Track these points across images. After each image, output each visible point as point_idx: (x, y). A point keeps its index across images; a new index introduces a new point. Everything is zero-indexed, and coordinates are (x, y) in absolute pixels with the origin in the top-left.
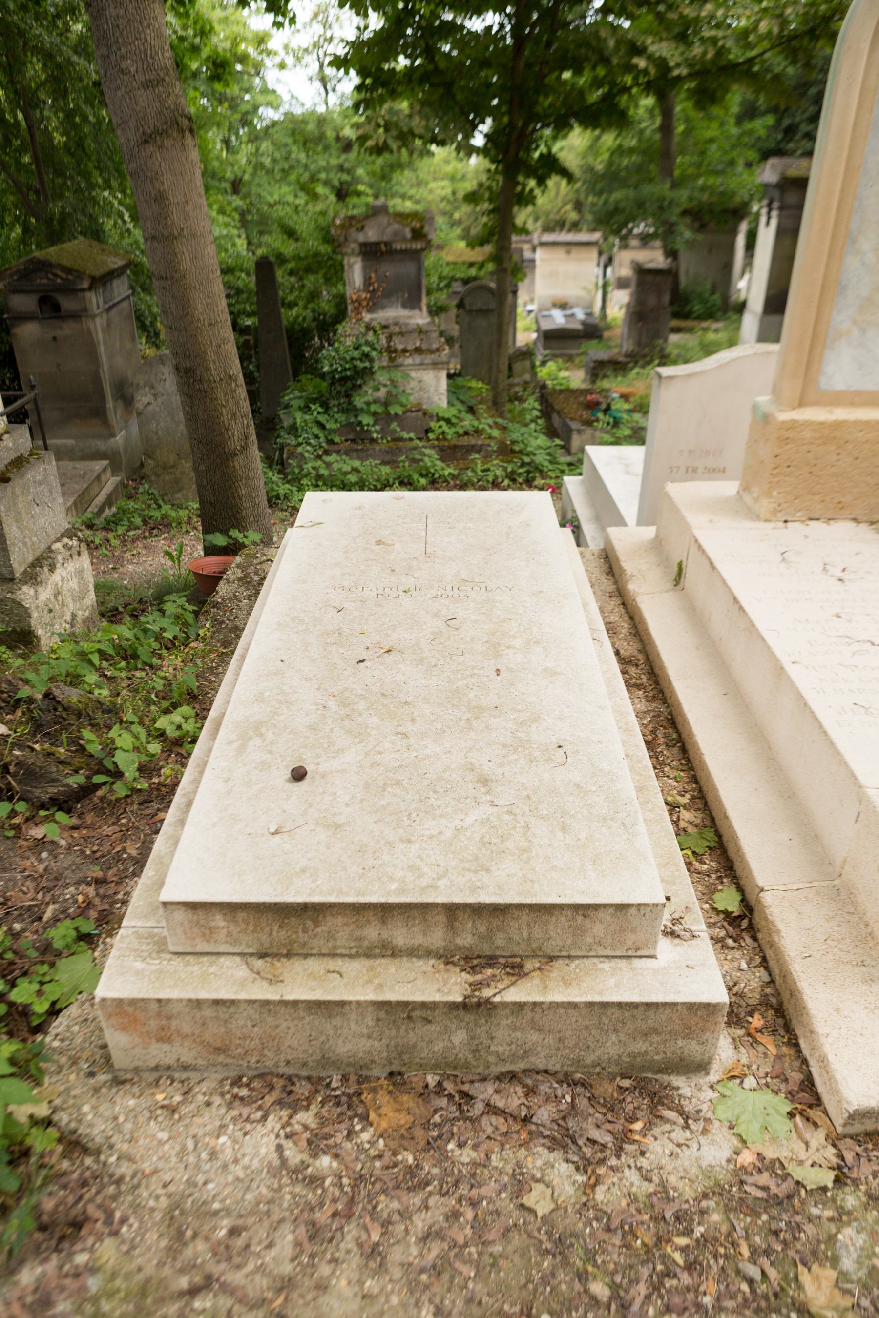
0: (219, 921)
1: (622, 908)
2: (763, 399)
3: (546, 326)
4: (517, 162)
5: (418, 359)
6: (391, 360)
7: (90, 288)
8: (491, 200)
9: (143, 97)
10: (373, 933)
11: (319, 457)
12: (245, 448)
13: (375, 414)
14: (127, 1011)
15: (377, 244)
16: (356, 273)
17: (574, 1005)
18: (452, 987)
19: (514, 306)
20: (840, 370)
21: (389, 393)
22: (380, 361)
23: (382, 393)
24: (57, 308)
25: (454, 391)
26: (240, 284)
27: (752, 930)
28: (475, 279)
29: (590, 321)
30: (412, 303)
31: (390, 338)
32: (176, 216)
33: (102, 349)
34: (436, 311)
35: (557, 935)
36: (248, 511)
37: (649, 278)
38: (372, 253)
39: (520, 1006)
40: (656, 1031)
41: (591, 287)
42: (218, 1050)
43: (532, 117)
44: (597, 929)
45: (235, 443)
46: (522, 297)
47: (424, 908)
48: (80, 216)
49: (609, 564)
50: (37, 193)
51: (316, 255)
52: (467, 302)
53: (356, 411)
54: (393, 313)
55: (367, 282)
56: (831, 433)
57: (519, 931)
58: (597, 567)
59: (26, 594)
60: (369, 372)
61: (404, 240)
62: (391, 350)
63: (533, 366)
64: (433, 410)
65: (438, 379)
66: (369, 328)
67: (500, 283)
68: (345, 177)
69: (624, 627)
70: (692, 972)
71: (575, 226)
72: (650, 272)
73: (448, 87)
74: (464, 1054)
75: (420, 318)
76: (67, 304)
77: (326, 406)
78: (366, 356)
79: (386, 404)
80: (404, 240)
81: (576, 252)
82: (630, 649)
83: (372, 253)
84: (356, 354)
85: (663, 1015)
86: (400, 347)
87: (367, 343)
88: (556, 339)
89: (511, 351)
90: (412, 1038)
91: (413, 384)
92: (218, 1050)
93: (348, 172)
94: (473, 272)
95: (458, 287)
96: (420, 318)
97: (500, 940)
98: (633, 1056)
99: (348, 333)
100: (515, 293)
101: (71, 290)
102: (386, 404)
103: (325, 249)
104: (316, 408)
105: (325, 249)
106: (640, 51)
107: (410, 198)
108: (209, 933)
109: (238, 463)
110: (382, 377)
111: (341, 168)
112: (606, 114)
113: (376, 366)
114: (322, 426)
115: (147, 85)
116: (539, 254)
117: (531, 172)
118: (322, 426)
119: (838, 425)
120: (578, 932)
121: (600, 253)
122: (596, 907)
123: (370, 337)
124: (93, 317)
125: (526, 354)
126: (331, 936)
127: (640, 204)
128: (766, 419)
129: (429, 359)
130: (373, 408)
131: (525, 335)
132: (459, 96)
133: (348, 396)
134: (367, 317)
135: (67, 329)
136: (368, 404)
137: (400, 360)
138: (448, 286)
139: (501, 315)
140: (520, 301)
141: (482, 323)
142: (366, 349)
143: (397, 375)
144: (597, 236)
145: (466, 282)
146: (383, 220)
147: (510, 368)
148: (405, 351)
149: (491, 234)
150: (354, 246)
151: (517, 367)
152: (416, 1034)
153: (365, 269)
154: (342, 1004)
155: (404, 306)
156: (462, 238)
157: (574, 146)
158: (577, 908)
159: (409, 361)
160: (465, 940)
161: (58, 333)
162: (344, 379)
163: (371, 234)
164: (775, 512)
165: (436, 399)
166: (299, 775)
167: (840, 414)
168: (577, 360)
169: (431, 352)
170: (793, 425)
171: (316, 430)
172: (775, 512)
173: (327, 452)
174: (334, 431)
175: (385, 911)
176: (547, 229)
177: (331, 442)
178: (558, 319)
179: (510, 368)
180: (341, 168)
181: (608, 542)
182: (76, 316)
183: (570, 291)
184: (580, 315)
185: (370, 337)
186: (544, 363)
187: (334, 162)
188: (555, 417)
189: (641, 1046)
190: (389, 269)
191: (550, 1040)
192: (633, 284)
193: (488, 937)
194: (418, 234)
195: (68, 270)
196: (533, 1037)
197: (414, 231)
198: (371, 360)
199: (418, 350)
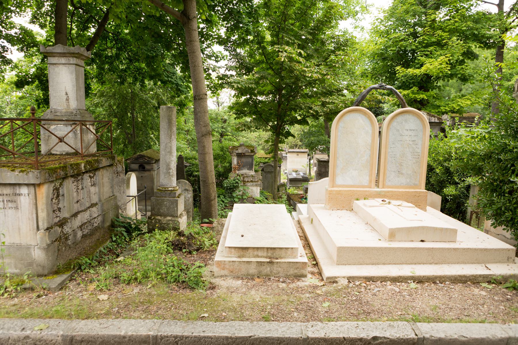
0: (233, 250)
1: (292, 248)
2: (327, 187)
3: (290, 177)
4: (279, 134)
5: (251, 184)
6: (244, 184)
7: (155, 163)
8: (272, 142)
9: (203, 129)
10: (256, 253)
11: (222, 210)
12: (215, 199)
13: (239, 198)
14: (219, 263)
15: (241, 153)
16: (235, 161)
17: (285, 262)
18: (268, 260)
19: (280, 171)
20: (339, 181)
21: (243, 193)
22: (241, 184)
23: (241, 193)
24: (144, 168)
25: (261, 193)
26: (194, 162)
27: (317, 266)
28: (267, 162)
29: (305, 176)
30: (250, 168)
31: (244, 178)
32: (206, 150)
33: (155, 180)
34: (256, 171)
35: (283, 253)
36: (214, 214)
37: (322, 163)
38: (239, 155)
39: (278, 262)
40: (298, 268)
41: (306, 166)
42: (232, 272)
43: (283, 121)
44: (289, 252)
45: (213, 198)
46: (283, 168)
47: (263, 248)
48: (146, 142)
49: (299, 222)
50: (131, 135)
51: (218, 155)
52: (264, 169)
53: (233, 197)
54: (245, 171)
55: (238, 163)
56: (339, 193)
57: (277, 252)
58: (297, 223)
59: (179, 220)
60: (237, 187)
61: (249, 153)
62: (244, 182)
63: (286, 189)
64: (256, 198)
65: (257, 189)
66: (238, 175)
67: (275, 164)
68: (224, 130)
69: (301, 232)
70: (302, 257)
71: (300, 147)
72: (322, 161)
73: (260, 115)
74: (269, 273)
75: (252, 173)
76: (147, 167)
77: (225, 196)
78: (237, 182)
79: (242, 196)
80: (249, 153)
81: (300, 154)
82: (301, 235)
83: (239, 155)
84: (234, 182)
85: (299, 264)
86: (247, 180)
87: (237, 179)
88: (293, 181)
89: (278, 184)
90: (261, 269)
91: (250, 190)
92: (232, 272)
93: (225, 129)
94: (267, 160)
95: (261, 165)
96: (252, 173)
97: (275, 255)
98: (295, 273)
99: (232, 176)
100: (280, 167)
101: (149, 163)
102: (242, 196)
103: (221, 153)
104: (222, 197)
105: (221, 153)
106: (311, 108)
107: (245, 137)
108: (231, 253)
109: (213, 202)
110: (241, 188)
111: (223, 128)
112: (303, 122)
113: (240, 185)
114: (223, 202)
115: (204, 126)
116: (288, 155)
117: (283, 135)
118: (223, 202)
119: (340, 191)
120: (286, 253)
121: (308, 155)
122: (288, 248)
123: (238, 177)
124: (154, 171)
125: (283, 185)
126: (249, 254)
127: (319, 142)
128: (327, 190)
129: (255, 184)
130: (238, 197)
131: (283, 179)
132: (263, 117)
133: (231, 193)
134: (237, 172)
135: (146, 174)
136: (237, 195)
137: (246, 184)
138: (259, 164)
139: (275, 173)
140: (282, 170)
141: (269, 175)
142: (237, 181)
143: (245, 188)
144: (307, 150)
145: (264, 163)
146: (243, 147)
147: (278, 189)
148: (248, 181)
149: (272, 151)
150: (235, 154)
151: (281, 189)
152: (262, 268)
153: (237, 159)
154: (251, 262)
155: (248, 169)
156: (263, 149)
157: (296, 129)
158: (286, 248)
159: (249, 184)
160: (269, 254)
161: (142, 175)
162: (230, 189)
163: (240, 151)
164: (330, 208)
165: (256, 195)
166: (242, 236)
167: (340, 189)
168: (301, 188)
169: (255, 182)
170: (331, 191)
171: (222, 203)
172: (330, 208)
173: (224, 209)
174: (227, 203)
175: (258, 248)
176: (291, 147)
177: (226, 206)
178: (294, 175)
179: (278, 189)
180: (223, 128)
181: (299, 219)
182: (149, 170)
183: (298, 167)
184: (302, 174)
185: (238, 177)
186: (289, 189)
187: (220, 125)
188: (291, 201)
189: (296, 271)
190: (244, 160)
191: (282, 270)
192: (317, 165)
193: (273, 254)
194: (252, 151)
195: (149, 158)
196: (280, 269)
197: (251, 150)
198: (238, 184)
199: (252, 181)
